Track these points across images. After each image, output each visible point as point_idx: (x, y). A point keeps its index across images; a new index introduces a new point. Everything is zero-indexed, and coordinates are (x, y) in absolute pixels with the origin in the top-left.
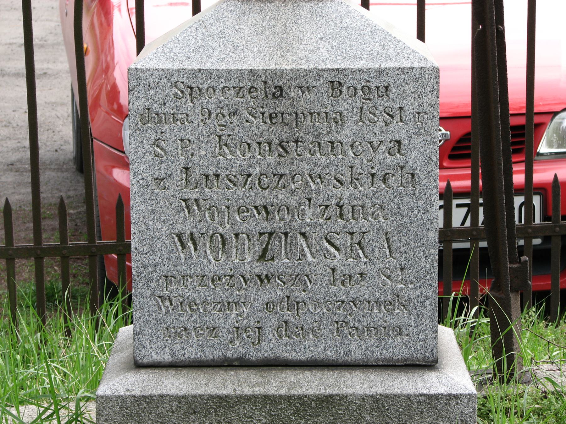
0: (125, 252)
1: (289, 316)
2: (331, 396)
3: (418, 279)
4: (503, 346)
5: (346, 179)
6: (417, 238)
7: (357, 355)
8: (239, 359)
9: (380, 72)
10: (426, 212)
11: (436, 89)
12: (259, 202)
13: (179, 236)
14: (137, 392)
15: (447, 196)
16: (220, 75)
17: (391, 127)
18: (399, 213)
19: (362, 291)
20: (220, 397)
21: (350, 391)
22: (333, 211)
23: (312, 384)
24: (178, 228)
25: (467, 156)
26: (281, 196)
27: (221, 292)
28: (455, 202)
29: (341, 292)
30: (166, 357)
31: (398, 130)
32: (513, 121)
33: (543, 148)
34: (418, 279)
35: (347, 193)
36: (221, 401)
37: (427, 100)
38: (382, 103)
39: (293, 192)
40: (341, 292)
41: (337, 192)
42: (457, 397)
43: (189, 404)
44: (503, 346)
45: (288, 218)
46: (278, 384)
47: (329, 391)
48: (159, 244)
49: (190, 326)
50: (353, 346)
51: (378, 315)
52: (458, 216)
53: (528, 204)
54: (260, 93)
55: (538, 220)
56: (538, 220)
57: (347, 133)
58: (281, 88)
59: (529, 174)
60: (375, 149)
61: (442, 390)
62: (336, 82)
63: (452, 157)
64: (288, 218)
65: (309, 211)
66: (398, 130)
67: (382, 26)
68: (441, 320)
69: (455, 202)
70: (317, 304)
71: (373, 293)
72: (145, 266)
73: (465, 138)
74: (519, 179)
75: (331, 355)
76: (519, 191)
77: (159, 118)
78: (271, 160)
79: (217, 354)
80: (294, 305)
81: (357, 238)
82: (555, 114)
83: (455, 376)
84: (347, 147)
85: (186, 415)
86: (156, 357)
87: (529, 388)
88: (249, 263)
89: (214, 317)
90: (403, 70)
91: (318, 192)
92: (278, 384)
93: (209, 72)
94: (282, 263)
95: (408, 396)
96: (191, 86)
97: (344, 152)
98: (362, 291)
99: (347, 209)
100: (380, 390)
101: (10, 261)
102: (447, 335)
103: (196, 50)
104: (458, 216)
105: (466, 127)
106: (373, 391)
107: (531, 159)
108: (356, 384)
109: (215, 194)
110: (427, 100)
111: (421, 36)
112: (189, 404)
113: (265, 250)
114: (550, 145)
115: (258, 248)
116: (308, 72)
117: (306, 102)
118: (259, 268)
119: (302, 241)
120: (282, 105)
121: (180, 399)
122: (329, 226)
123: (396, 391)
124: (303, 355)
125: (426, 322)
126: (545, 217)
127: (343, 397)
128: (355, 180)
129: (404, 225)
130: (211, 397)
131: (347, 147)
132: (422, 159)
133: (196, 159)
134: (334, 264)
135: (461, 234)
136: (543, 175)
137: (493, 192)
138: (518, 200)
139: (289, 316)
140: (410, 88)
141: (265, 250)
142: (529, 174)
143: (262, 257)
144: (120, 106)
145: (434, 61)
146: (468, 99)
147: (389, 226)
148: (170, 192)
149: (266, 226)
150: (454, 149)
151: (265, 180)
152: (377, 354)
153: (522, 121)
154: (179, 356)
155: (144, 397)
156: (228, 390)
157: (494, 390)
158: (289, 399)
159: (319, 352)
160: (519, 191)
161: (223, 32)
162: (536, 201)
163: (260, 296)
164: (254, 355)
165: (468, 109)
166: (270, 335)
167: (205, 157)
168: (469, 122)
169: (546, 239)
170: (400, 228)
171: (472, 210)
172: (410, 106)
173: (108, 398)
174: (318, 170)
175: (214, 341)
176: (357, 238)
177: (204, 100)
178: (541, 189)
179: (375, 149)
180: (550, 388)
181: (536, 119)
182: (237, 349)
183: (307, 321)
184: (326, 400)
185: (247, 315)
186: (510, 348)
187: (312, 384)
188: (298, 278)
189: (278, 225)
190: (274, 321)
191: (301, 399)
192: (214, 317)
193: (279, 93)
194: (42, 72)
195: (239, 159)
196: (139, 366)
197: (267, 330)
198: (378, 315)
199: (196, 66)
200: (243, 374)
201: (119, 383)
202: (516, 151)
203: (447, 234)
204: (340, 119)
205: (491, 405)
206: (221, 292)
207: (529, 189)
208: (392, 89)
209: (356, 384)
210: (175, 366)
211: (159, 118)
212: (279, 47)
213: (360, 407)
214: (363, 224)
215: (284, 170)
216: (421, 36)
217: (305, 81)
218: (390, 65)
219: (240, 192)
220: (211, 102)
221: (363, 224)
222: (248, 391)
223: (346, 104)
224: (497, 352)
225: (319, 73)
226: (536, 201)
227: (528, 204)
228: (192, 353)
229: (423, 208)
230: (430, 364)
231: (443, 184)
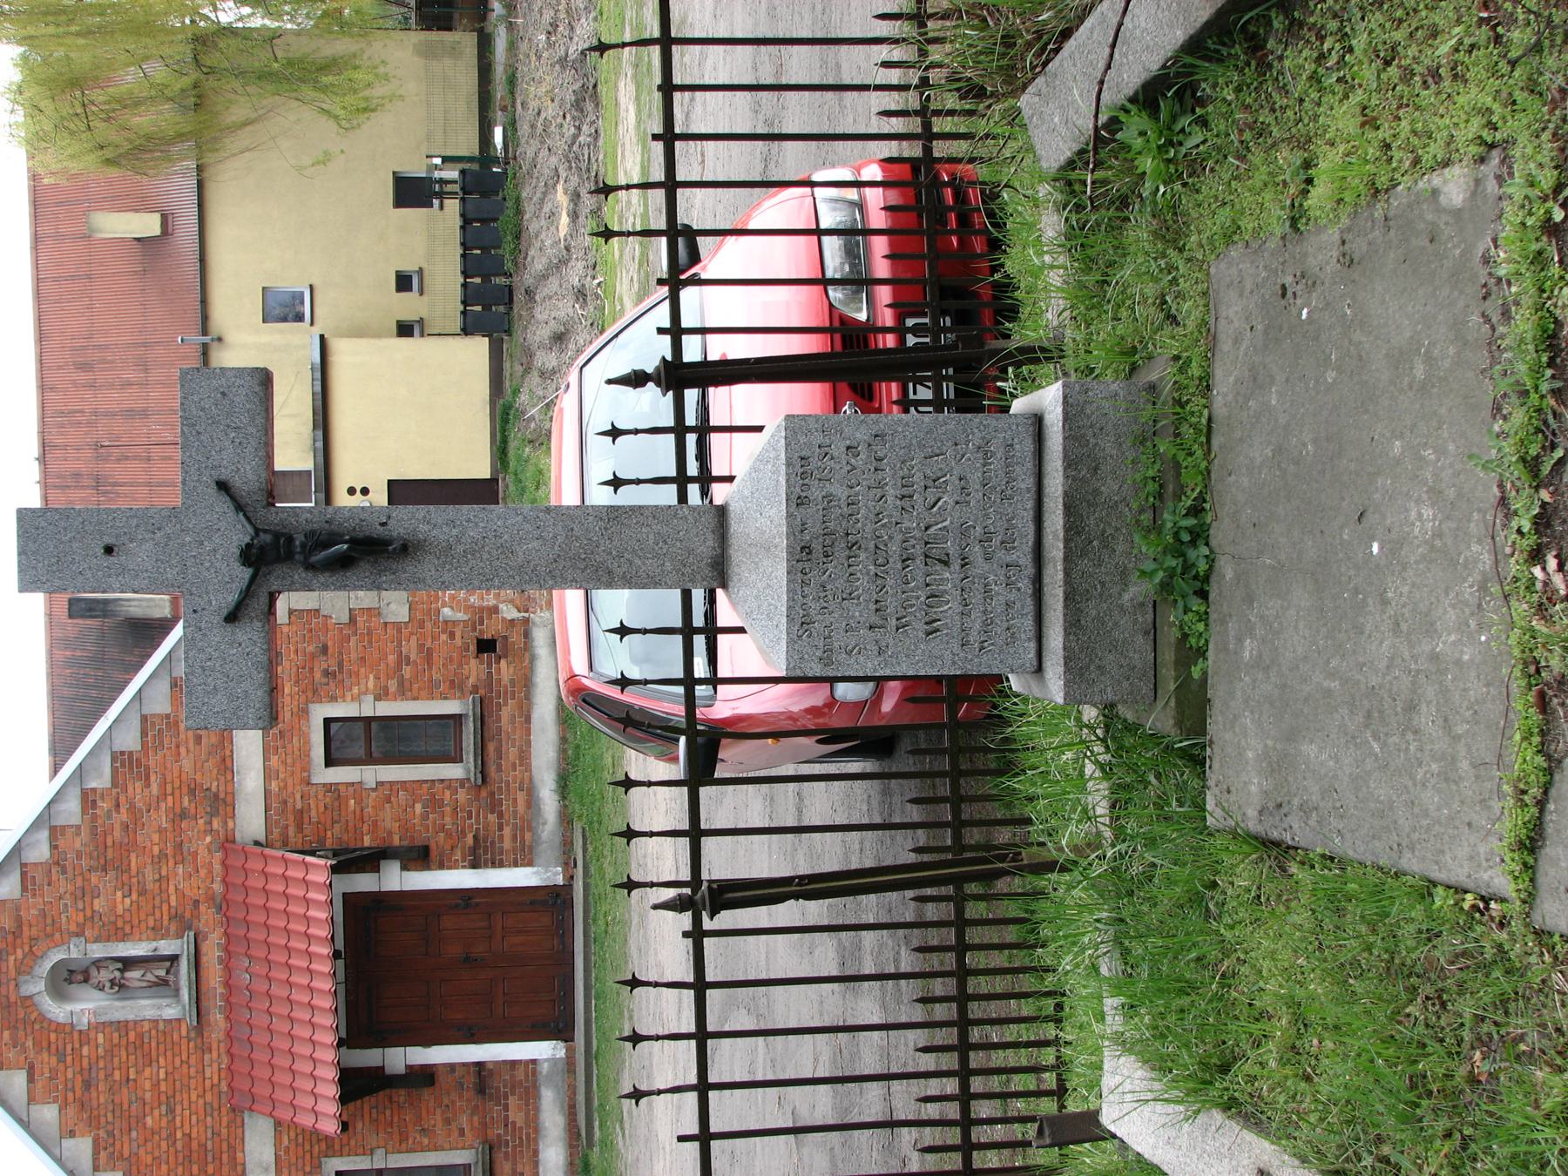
0: (938, 679)
1: (996, 541)
2: (1065, 504)
3: (965, 431)
4: (1032, 355)
5: (879, 493)
6: (930, 432)
7: (1030, 482)
8: (1034, 584)
9: (789, 464)
10: (907, 424)
11: (804, 418)
12: (899, 566)
13: (928, 634)
14: (1061, 669)
15: (905, 404)
16: (791, 599)
17: (836, 454)
18: (909, 447)
19: (975, 478)
20: (1066, 599)
21: (1060, 489)
22: (906, 503)
23: (1055, 520)
24: (921, 635)
25: (870, 387)
26: (894, 548)
27: (976, 598)
28: (912, 396)
29: (976, 496)
30: (1032, 645)
31: (838, 449)
32: (838, 348)
33: (863, 316)
34: (965, 431)
35: (891, 492)
36: (1069, 598)
37: (813, 425)
38: (815, 462)
39: (891, 538)
40: (976, 496)
41: (890, 500)
42: (1065, 397)
43: (1071, 625)
44: (1032, 355)
45: (913, 542)
46: (1055, 550)
47: (1061, 506)
48: (936, 652)
49: (1005, 625)
50: (1023, 486)
51: (996, 464)
52: (925, 393)
53: (916, 330)
54: (807, 565)
55: (926, 320)
56: (926, 320)
57: (840, 492)
58: (803, 548)
59: (886, 330)
60: (854, 468)
61: (1060, 409)
62: (797, 501)
63: (871, 398)
64: (913, 542)
65: (907, 524)
66: (838, 449)
67: (750, 463)
68: (1005, 409)
69: (912, 396)
70: (987, 516)
71: (977, 469)
72: (954, 663)
73: (853, 387)
74: (890, 341)
75: (1030, 504)
76: (901, 340)
77: (828, 650)
78: (863, 556)
79: (1029, 601)
80: (987, 537)
81: (930, 483)
82: (831, 304)
83: (1049, 398)
84: (852, 492)
85: (1081, 628)
86: (1032, 655)
87: (1068, 333)
88: (950, 575)
89: (997, 604)
90: (787, 445)
91: (891, 516)
92: (1055, 550)
93: (789, 608)
94: (950, 546)
95: (1065, 438)
96: (801, 623)
97: (857, 494)
98: (975, 478)
99: (905, 491)
100: (1060, 463)
101: (962, 799)
102: (1017, 406)
103: (771, 619)
104: (925, 393)
105: (843, 387)
106: (1061, 469)
107: (871, 328)
108: (1055, 484)
109: (892, 604)
110: (813, 425)
111: (759, 429)
112: (1071, 625)
113: (940, 561)
114: (860, 310)
115: (939, 567)
116: (789, 525)
117: (815, 527)
118: (956, 566)
119: (932, 530)
120: (817, 547)
121: (1067, 633)
122: (920, 507)
123: (1060, 448)
124: (1030, 529)
125: (1013, 420)
126: (924, 315)
127: (1066, 494)
128: (880, 485)
129: (919, 443)
130: (1066, 606)
131: (852, 492)
132: (863, 428)
133: (862, 620)
134: (951, 502)
135: (938, 391)
136: (887, 318)
137: (903, 365)
138: (911, 340)
139: (996, 541)
140: (803, 439)
141: (940, 561)
142: (886, 330)
143: (946, 563)
144: (825, 705)
145: (780, 419)
146: (818, 386)
147: (919, 456)
148: (891, 642)
149: (919, 561)
150: (863, 396)
151: (880, 561)
152: (1029, 465)
153: (837, 337)
154: (1031, 634)
155: (1066, 664)
156: (1060, 593)
157: (1070, 363)
158: (1067, 541)
159: (1028, 515)
160: (901, 340)
161: (757, 597)
162: (910, 322)
163: (979, 566)
164: (1030, 571)
165: (827, 386)
166: (1013, 557)
167: (861, 612)
168: (838, 385)
169: (944, 313)
170: (922, 446)
171: (920, 381)
172: (818, 439)
173: (1066, 694)
174: (872, 516)
175: (1018, 605)
176: (930, 483)
177: (813, 612)
178: (900, 318)
179: (854, 468)
180: (1067, 314)
181: (836, 324)
182: (1025, 585)
183: (1001, 525)
184: (1069, 509)
185: (996, 577)
186: (1032, 350)
187: (1055, 520)
188: (964, 531)
189: (919, 550)
190: (1001, 554)
191: (1067, 530)
192: (997, 604)
193: (806, 549)
194: (804, 794)
195: (863, 582)
196: (1039, 669)
197: (1008, 559)
198: (996, 464)
199: (784, 620)
200: (1046, 580)
201: (1055, 687)
202: (866, 344)
203: (938, 404)
204: (829, 497)
205: (1082, 365)
206: (976, 598)
207: (900, 330)
208: (803, 453)
209: (1055, 484)
210: (1039, 638)
211: (828, 650)
212: (768, 550)
213: (1074, 479)
214: (918, 477)
215: (872, 545)
216: (759, 429)
217: (796, 529)
218: (783, 456)
219: (890, 582)
220: (814, 607)
221: (918, 477)
222: (1061, 575)
223: (816, 493)
224: (1037, 361)
225: (789, 515)
226: (910, 322)
227: (916, 330)
228: (1029, 623)
229: (910, 427)
230: (1038, 420)
231: (895, 408)
